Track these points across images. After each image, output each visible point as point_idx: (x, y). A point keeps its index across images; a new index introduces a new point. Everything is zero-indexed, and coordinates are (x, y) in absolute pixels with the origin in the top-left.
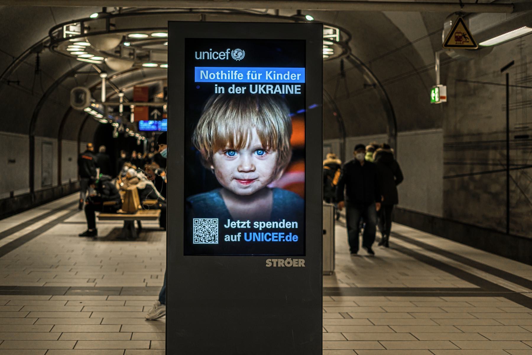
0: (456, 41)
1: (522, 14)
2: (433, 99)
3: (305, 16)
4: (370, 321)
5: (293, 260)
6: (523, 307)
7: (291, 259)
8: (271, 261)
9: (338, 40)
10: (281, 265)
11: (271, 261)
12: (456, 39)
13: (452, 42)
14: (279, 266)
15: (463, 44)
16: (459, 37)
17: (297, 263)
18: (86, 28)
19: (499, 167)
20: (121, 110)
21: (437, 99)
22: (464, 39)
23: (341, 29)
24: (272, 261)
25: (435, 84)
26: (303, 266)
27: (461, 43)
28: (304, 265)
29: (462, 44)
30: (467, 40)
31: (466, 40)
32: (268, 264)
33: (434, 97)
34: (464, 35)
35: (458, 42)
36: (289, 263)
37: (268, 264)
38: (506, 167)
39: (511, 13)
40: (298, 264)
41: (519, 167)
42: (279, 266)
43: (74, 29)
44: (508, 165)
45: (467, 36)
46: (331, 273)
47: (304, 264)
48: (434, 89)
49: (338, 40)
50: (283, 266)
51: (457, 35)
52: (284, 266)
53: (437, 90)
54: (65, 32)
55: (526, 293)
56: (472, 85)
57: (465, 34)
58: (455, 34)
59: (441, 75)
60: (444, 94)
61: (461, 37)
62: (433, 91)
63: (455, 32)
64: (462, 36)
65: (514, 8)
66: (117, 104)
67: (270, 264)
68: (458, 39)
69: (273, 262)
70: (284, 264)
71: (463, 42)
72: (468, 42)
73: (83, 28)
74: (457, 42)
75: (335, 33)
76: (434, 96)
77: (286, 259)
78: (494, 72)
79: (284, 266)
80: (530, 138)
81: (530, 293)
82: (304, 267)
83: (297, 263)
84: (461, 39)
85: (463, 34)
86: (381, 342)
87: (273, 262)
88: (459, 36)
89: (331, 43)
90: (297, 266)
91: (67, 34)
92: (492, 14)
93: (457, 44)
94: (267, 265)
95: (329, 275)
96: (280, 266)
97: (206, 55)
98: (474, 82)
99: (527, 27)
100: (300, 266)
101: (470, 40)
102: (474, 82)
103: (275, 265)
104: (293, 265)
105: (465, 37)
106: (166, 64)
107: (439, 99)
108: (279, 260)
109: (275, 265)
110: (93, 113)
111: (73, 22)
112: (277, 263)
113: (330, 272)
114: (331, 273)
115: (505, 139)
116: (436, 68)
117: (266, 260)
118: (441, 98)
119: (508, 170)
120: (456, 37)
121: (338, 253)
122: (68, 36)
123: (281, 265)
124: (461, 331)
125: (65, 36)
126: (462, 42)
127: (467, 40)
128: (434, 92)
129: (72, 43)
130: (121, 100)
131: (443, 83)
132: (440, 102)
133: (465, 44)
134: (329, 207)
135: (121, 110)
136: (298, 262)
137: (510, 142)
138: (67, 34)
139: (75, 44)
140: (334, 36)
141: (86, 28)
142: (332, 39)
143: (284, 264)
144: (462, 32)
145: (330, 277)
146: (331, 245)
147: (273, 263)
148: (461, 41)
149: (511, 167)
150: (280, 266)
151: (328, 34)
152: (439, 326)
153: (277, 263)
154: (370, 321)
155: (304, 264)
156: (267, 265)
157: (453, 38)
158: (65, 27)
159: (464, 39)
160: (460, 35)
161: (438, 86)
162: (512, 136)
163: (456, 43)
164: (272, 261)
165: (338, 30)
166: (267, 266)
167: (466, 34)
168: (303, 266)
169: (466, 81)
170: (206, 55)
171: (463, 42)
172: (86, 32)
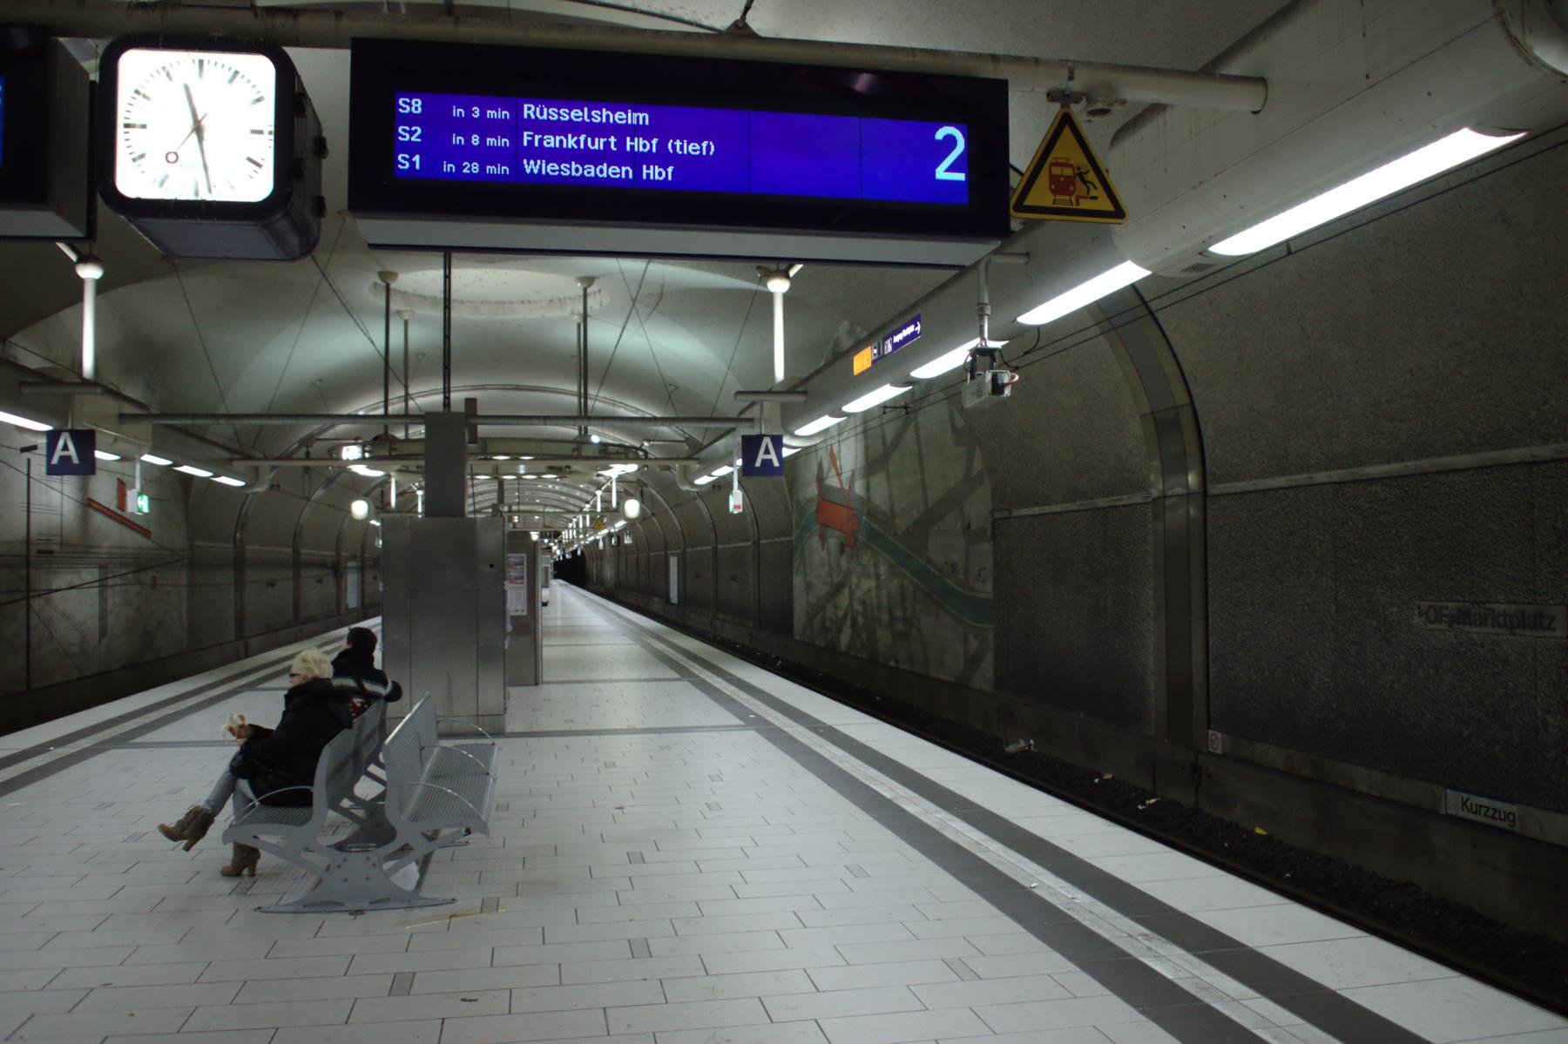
0: (1054, 192)
6: (728, 728)
15: (1078, 204)
19: (18, 596)
22: (1080, 188)
34: (1081, 175)
38: (25, 594)
41: (43, 592)
44: (28, 591)
45: (1091, 176)
51: (1056, 171)
57: (1082, 170)
58: (1050, 170)
61: (1070, 180)
63: (1050, 160)
68: (1060, 186)
71: (1078, 198)
72: (1096, 198)
74: (1058, 197)
80: (55, 555)
85: (1077, 172)
86: (1071, 996)
88: (1062, 176)
97: (561, 141)
101: (1100, 192)
105: (1085, 182)
115: (24, 552)
119: (27, 598)
124: (1241, 1004)
125: (758, 464)
126: (1073, 199)
127: (1093, 193)
133: (1086, 205)
137: (32, 558)
146: (710, 731)
148: (1070, 194)
149: (32, 594)
157: (1043, 180)
159: (1080, 188)
160: (1068, 172)
162: (33, 549)
170: (561, 141)
171: (1078, 198)
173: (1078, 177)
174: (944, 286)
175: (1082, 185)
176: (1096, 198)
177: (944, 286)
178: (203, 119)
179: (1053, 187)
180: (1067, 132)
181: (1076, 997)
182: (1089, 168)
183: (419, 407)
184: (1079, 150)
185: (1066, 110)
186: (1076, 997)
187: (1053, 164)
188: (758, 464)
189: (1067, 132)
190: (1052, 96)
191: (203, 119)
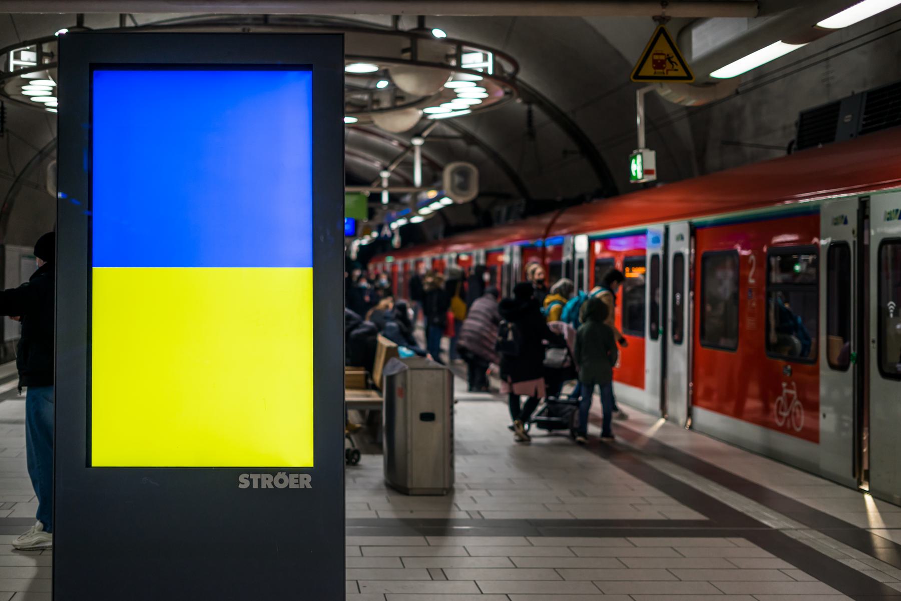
0: (655, 68)
1: (771, 19)
2: (634, 174)
3: (431, 30)
4: (680, 554)
5: (290, 475)
6: (773, 558)
7: (286, 474)
8: (248, 477)
9: (490, 72)
10: (267, 486)
11: (248, 477)
12: (654, 66)
13: (648, 70)
14: (263, 486)
15: (667, 73)
16: (659, 61)
17: (297, 481)
18: (47, 55)
20: (385, 198)
21: (640, 175)
22: (668, 65)
23: (495, 53)
24: (251, 478)
25: (636, 146)
26: (309, 486)
27: (664, 73)
28: (309, 485)
29: (665, 75)
30: (675, 67)
31: (673, 66)
32: (243, 484)
33: (636, 171)
34: (669, 59)
35: (658, 71)
36: (281, 481)
37: (243, 484)
39: (755, 17)
40: (299, 483)
42: (263, 486)
43: (28, 57)
45: (675, 59)
46: (445, 493)
47: (310, 483)
48: (635, 157)
49: (490, 72)
50: (271, 486)
51: (656, 57)
52: (272, 487)
53: (639, 158)
54: (13, 62)
55: (791, 529)
56: (748, 151)
57: (670, 56)
59: (647, 132)
60: (652, 165)
61: (663, 62)
62: (633, 161)
63: (653, 51)
64: (666, 59)
65: (759, 8)
66: (374, 189)
67: (246, 485)
68: (658, 65)
69: (252, 479)
70: (273, 483)
71: (667, 70)
72: (676, 70)
73: (40, 56)
75: (485, 59)
76: (635, 170)
77: (277, 474)
78: (784, 128)
79: (272, 487)
81: (796, 530)
82: (309, 489)
83: (297, 481)
84: (664, 66)
85: (667, 57)
87: (252, 479)
89: (480, 78)
90: (297, 486)
91: (15, 66)
92: (728, 19)
93: (656, 75)
94: (240, 484)
95: (442, 495)
96: (265, 487)
98: (752, 145)
99: (782, 43)
100: (302, 487)
101: (679, 67)
102: (752, 145)
103: (255, 486)
104: (289, 485)
105: (671, 62)
106: (347, 124)
107: (643, 175)
108: (262, 475)
109: (255, 486)
110: (436, 206)
111: (24, 44)
112: (260, 481)
113: (444, 489)
114: (445, 493)
116: (638, 121)
117: (238, 478)
118: (646, 172)
120: (655, 62)
121: (466, 453)
122: (18, 69)
123: (267, 486)
125: (12, 70)
126: (665, 71)
127: (675, 67)
128: (636, 163)
129: (27, 82)
130: (385, 184)
131: (648, 146)
132: (644, 181)
133: (671, 74)
134: (441, 372)
135: (385, 198)
136: (299, 479)
138: (15, 66)
139: (31, 82)
140: (485, 65)
141: (47, 55)
142: (481, 70)
143: (273, 483)
144: (665, 52)
145: (443, 498)
147: (251, 481)
148: (663, 68)
150: (265, 487)
151: (474, 63)
152: (603, 595)
153: (260, 481)
154: (680, 554)
155: (310, 483)
156: (240, 484)
157: (649, 62)
158: (12, 53)
160: (662, 57)
161: (641, 151)
163: (655, 73)
164: (251, 478)
165: (490, 55)
166: (241, 486)
167: (672, 57)
168: (309, 486)
169: (738, 144)
171: (667, 70)
172: (47, 61)
173: (667, 61)
174: (721, 594)
175: (670, 64)
176: (676, 70)
177: (721, 594)
178: (426, 539)
179: (654, 66)
180: (662, 36)
181: (577, 557)
182: (674, 55)
183: (31, 579)
184: (668, 46)
185: (662, 26)
186: (577, 557)
187: (654, 54)
188: (12, 70)
189: (662, 36)
190: (655, 18)
191: (426, 539)
